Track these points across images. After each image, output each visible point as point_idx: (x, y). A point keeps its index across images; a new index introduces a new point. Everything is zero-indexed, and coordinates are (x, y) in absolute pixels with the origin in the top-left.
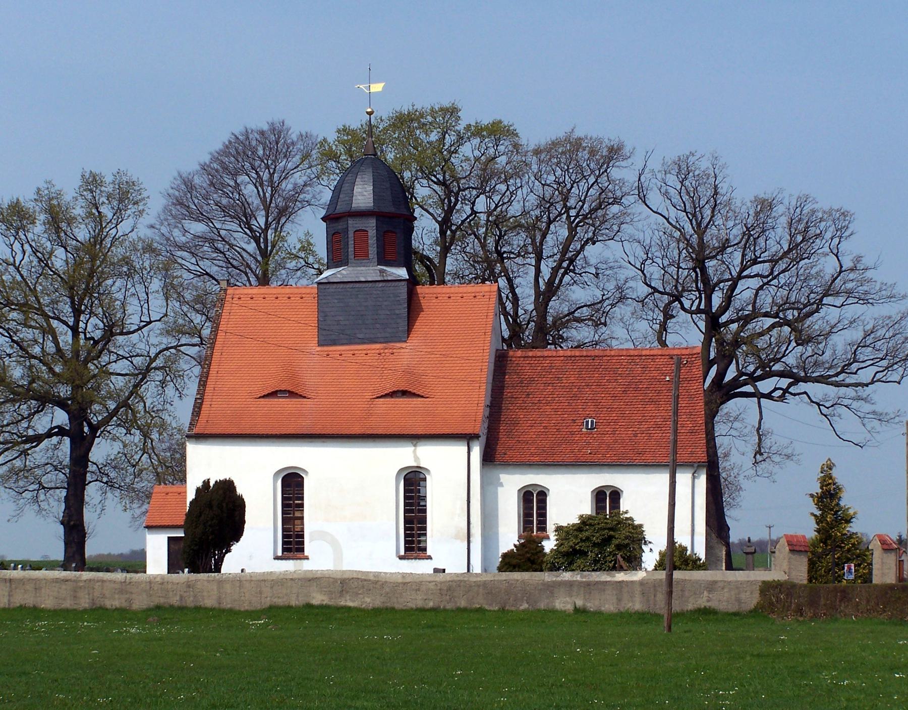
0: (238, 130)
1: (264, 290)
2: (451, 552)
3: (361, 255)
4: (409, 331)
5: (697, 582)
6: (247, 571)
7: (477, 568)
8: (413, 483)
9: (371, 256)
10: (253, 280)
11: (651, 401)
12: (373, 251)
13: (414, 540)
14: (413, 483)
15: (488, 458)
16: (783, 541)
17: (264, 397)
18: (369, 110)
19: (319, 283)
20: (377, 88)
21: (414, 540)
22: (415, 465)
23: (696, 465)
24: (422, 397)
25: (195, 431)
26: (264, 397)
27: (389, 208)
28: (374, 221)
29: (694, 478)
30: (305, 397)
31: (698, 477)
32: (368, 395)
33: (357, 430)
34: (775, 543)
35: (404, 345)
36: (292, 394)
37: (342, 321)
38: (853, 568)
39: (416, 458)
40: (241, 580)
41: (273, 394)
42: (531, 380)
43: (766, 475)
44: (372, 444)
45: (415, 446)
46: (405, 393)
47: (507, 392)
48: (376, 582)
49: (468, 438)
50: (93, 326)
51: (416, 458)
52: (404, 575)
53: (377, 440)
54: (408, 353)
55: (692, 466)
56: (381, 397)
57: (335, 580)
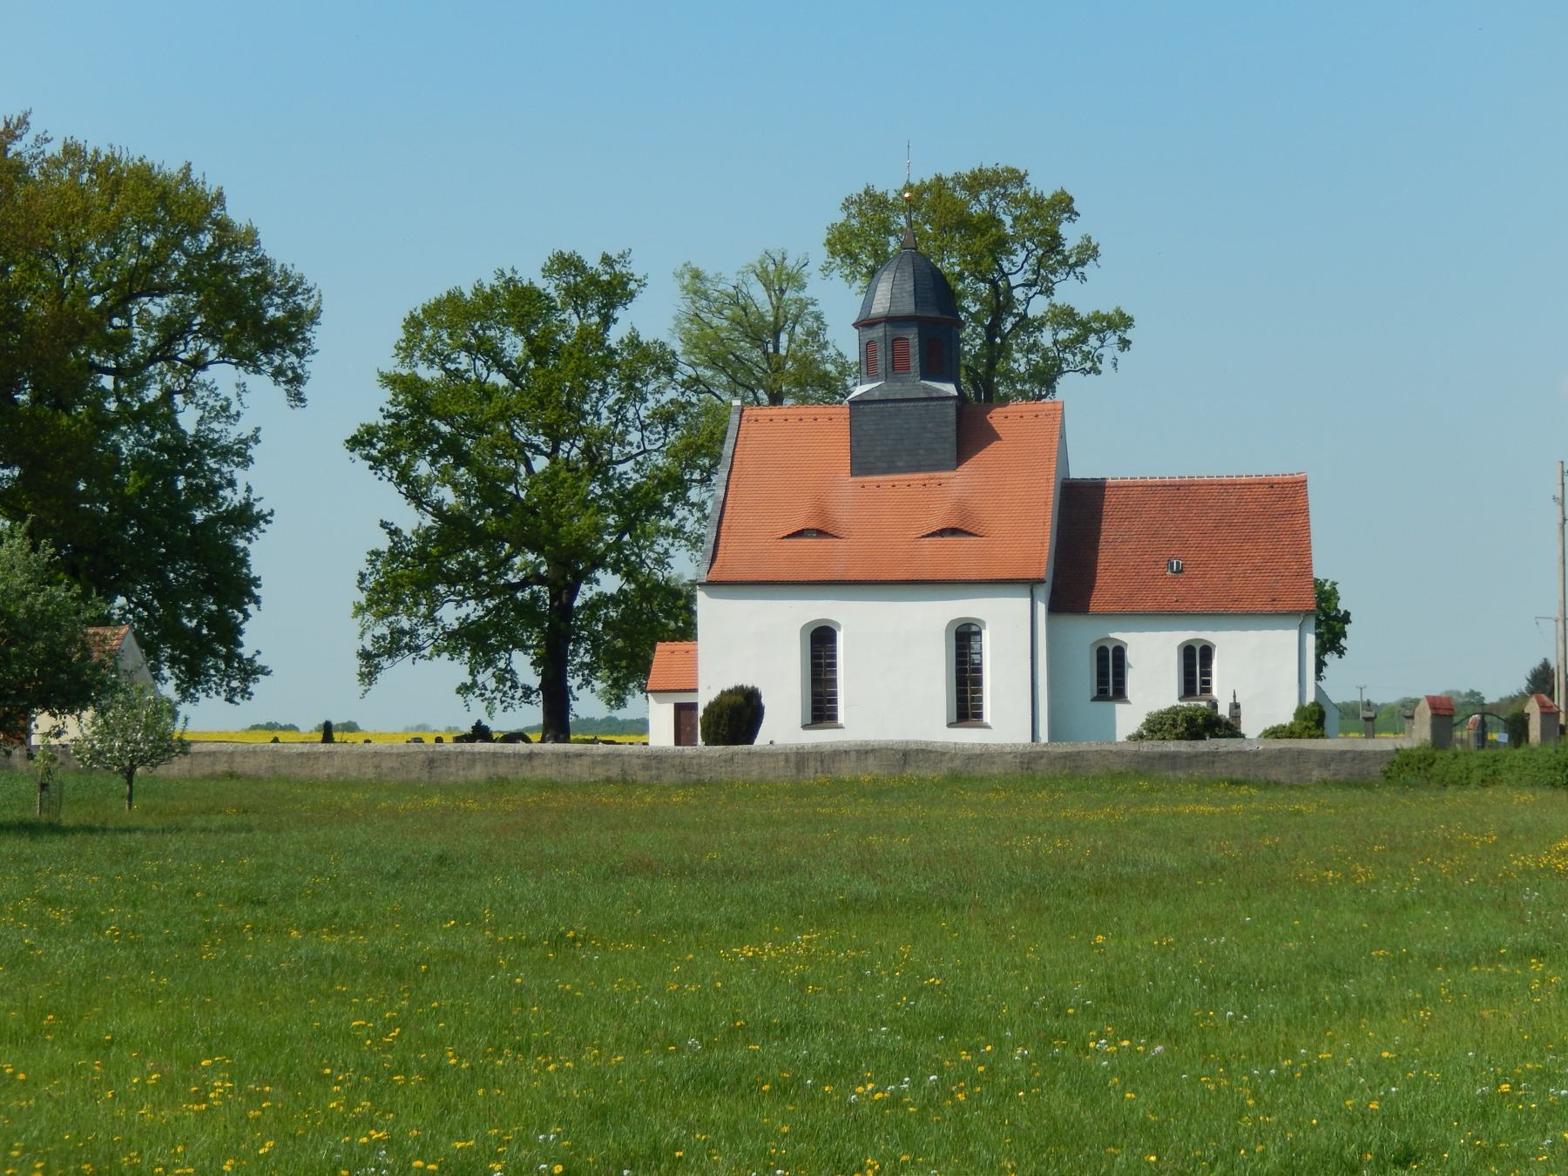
0: (209, 177)
1: (775, 410)
2: (1009, 717)
5: (1322, 753)
6: (777, 742)
7: (1044, 736)
8: (965, 638)
10: (762, 394)
12: (915, 363)
13: (966, 708)
14: (965, 638)
15: (1054, 609)
16: (1424, 705)
17: (789, 536)
19: (851, 402)
21: (966, 708)
25: (713, 576)
26: (789, 536)
32: (913, 534)
34: (1417, 702)
36: (821, 533)
37: (880, 445)
40: (770, 755)
41: (799, 534)
46: (954, 532)
48: (943, 754)
49: (1031, 584)
50: (571, 450)
52: (946, 745)
54: (960, 482)
56: (933, 534)
57: (897, 751)
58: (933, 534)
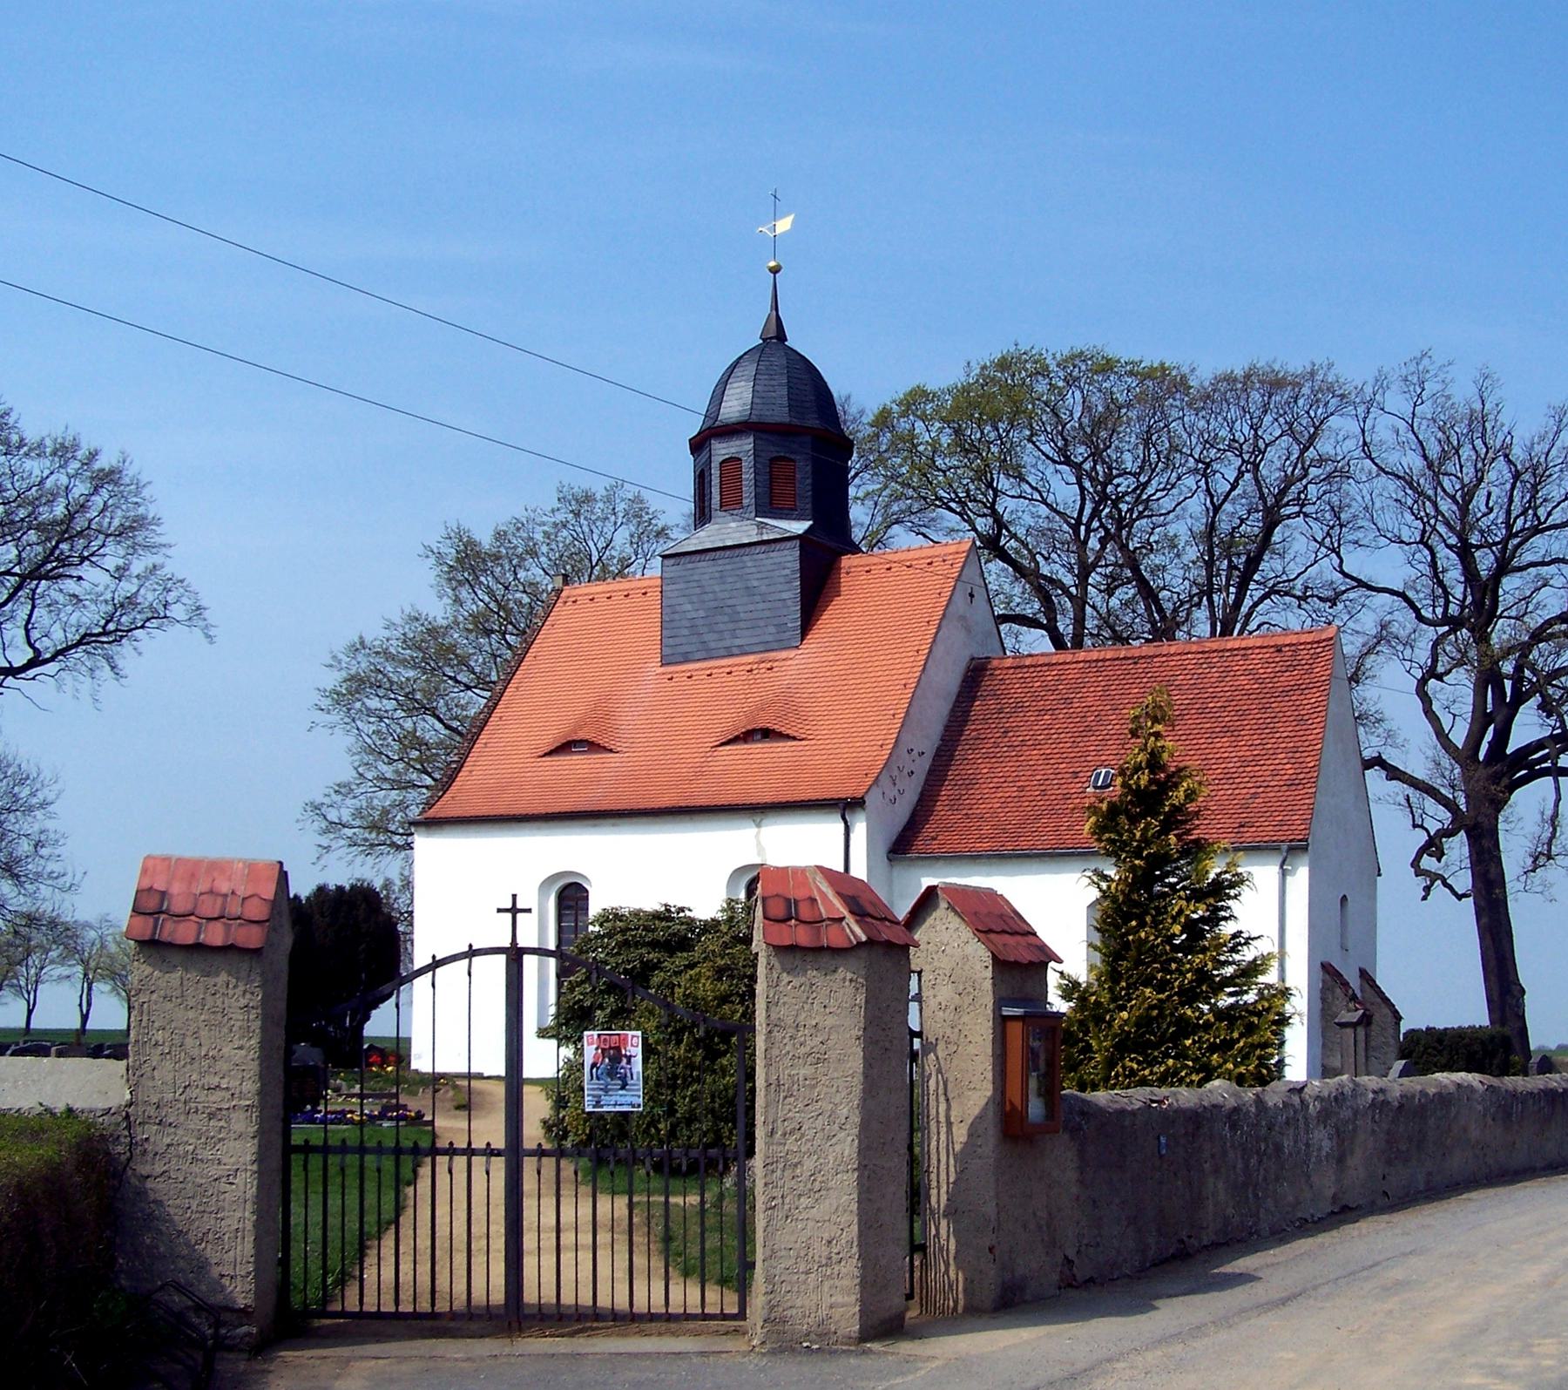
3: (731, 502)
4: (806, 627)
9: (746, 502)
11: (1226, 730)
17: (550, 753)
18: (772, 264)
20: (784, 225)
22: (758, 861)
23: (1285, 846)
24: (794, 738)
26: (550, 753)
27: (779, 412)
28: (751, 439)
29: (1284, 874)
30: (611, 751)
31: (1293, 872)
33: (666, 801)
35: (792, 653)
38: (635, 1049)
39: (761, 850)
42: (1019, 706)
43: (1539, 889)
44: (689, 825)
45: (758, 826)
46: (767, 734)
47: (970, 731)
51: (761, 850)
53: (696, 817)
54: (800, 664)
55: (1278, 849)
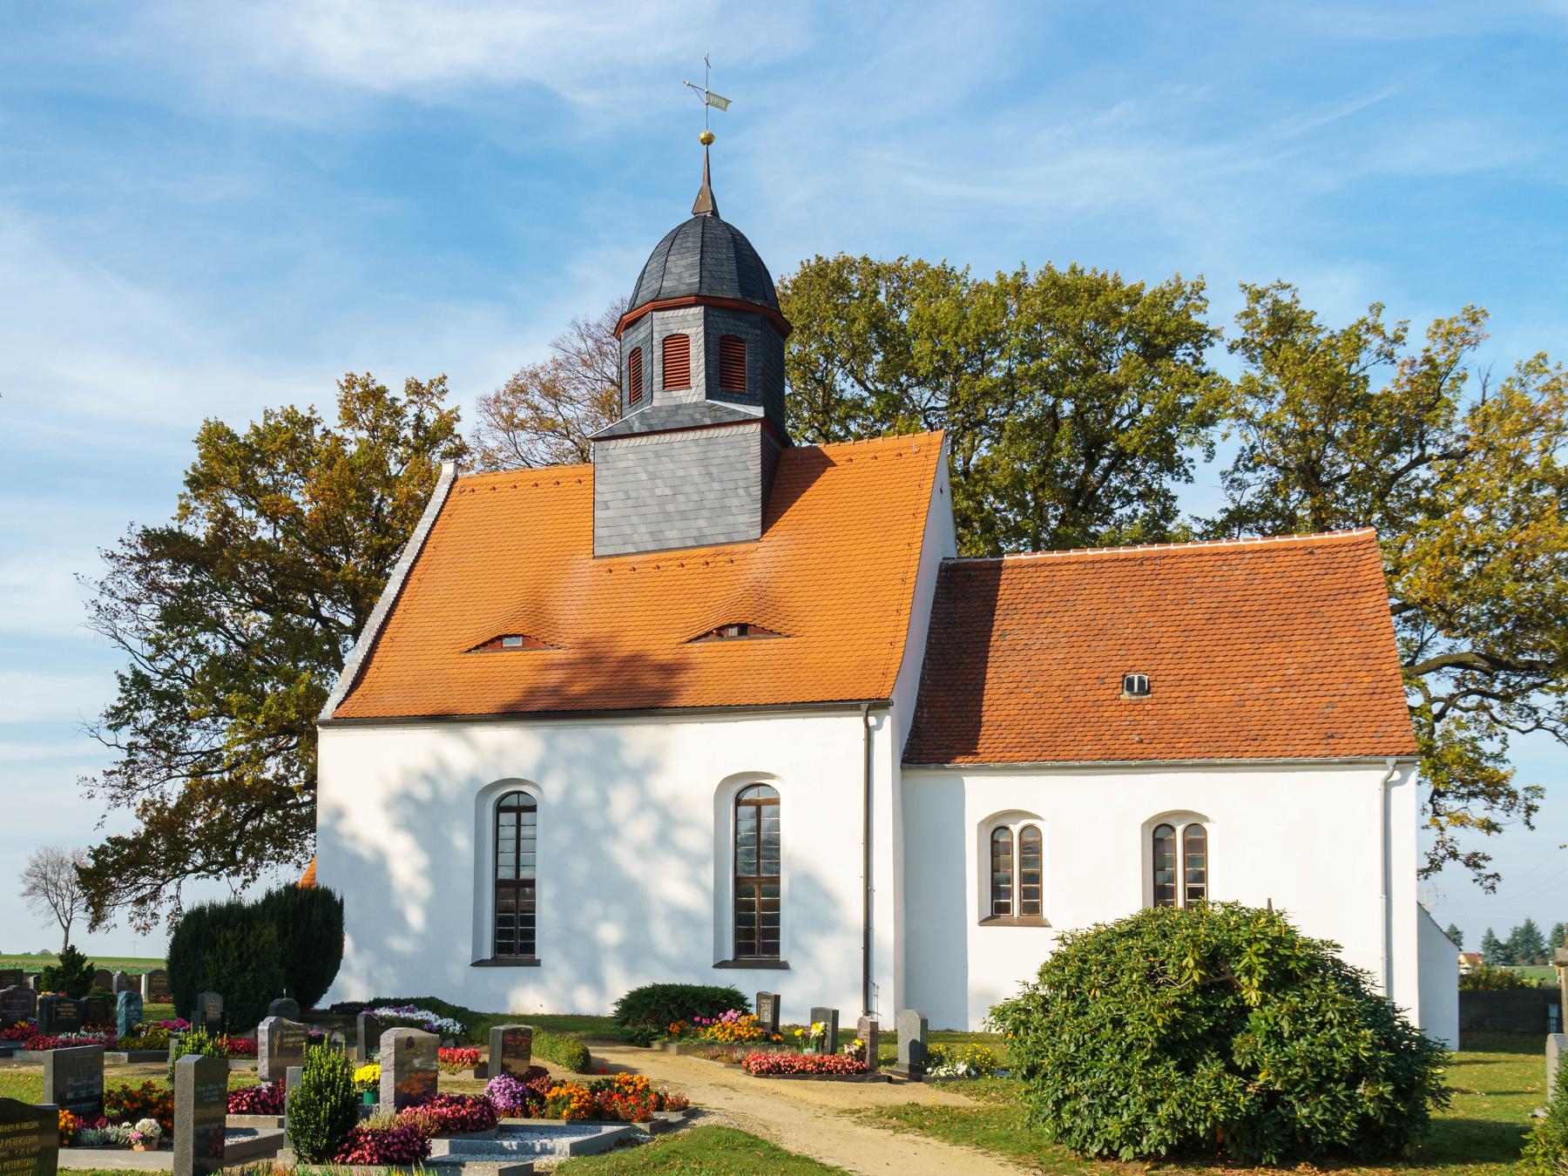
56: (698, 638)
58: (698, 638)
